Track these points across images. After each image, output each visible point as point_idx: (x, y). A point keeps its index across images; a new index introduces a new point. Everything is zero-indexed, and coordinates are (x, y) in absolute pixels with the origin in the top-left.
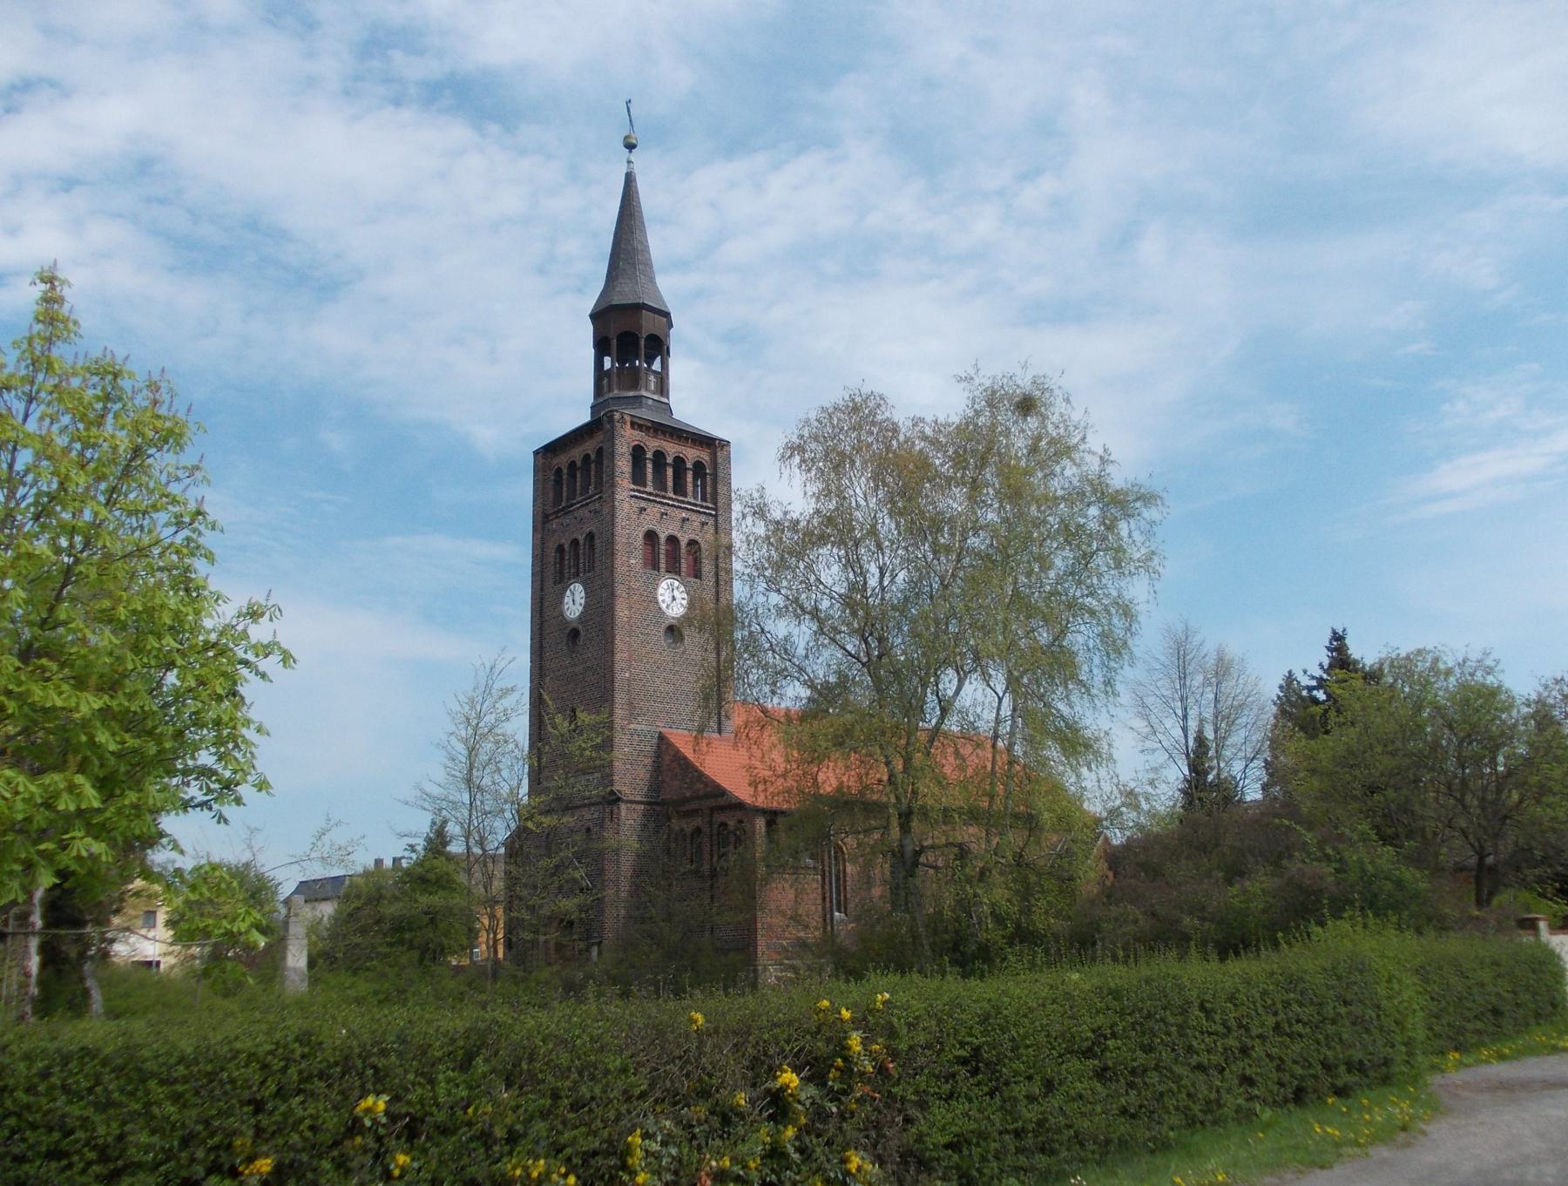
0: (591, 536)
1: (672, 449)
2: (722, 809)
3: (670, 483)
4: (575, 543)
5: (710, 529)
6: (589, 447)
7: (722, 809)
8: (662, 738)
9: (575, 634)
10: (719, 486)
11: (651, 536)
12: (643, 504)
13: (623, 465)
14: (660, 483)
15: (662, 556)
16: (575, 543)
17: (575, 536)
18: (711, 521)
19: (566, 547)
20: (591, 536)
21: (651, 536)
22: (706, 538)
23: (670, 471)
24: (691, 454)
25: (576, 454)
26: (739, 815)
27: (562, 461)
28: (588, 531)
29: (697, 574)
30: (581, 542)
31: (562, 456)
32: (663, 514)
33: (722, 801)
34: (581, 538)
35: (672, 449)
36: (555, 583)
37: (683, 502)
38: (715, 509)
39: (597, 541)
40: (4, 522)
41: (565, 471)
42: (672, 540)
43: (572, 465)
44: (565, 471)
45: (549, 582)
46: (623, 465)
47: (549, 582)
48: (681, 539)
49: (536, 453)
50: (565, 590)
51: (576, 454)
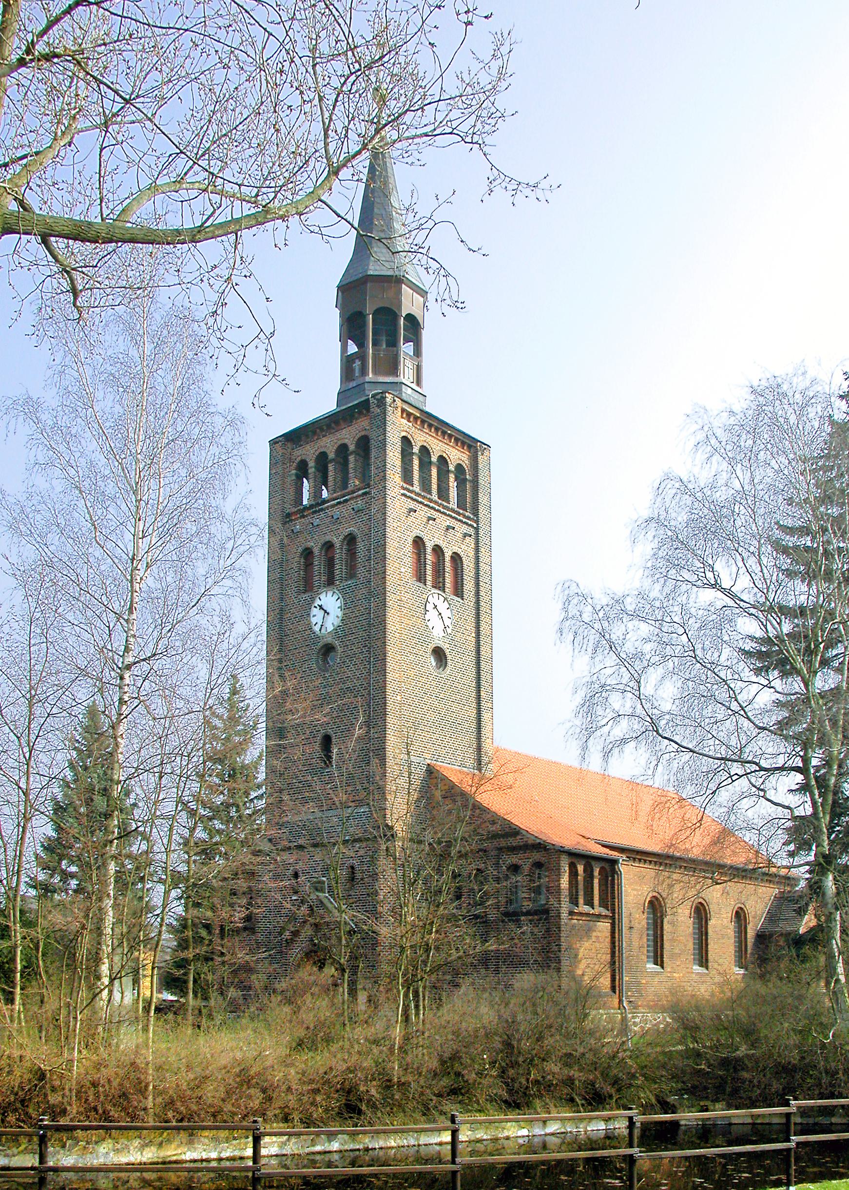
0: (351, 539)
1: (438, 447)
2: (513, 849)
3: (434, 487)
4: (329, 546)
5: (470, 541)
6: (348, 436)
7: (513, 849)
8: (431, 771)
9: (328, 649)
10: (480, 495)
11: (418, 542)
12: (413, 505)
13: (394, 457)
14: (426, 485)
15: (429, 567)
16: (329, 546)
17: (328, 538)
18: (472, 531)
19: (316, 551)
20: (351, 539)
21: (418, 542)
22: (466, 551)
23: (434, 472)
24: (456, 456)
25: (329, 444)
26: (537, 856)
27: (309, 452)
28: (347, 532)
29: (458, 591)
30: (337, 545)
31: (308, 447)
32: (429, 519)
33: (513, 842)
34: (337, 541)
35: (438, 447)
36: (299, 592)
37: (444, 507)
38: (477, 522)
39: (361, 546)
40: (7, 1108)
41: (311, 464)
42: (438, 550)
43: (343, 449)
44: (311, 464)
45: (291, 592)
46: (394, 457)
47: (291, 592)
48: (445, 550)
49: (273, 443)
50: (310, 604)
51: (329, 444)
